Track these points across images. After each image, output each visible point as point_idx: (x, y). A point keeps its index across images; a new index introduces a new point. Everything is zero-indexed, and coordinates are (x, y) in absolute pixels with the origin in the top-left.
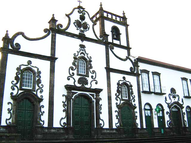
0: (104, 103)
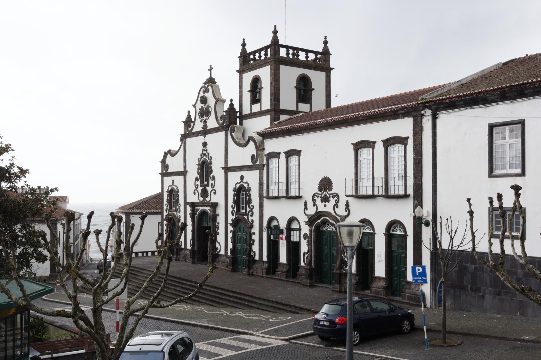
0: (221, 220)
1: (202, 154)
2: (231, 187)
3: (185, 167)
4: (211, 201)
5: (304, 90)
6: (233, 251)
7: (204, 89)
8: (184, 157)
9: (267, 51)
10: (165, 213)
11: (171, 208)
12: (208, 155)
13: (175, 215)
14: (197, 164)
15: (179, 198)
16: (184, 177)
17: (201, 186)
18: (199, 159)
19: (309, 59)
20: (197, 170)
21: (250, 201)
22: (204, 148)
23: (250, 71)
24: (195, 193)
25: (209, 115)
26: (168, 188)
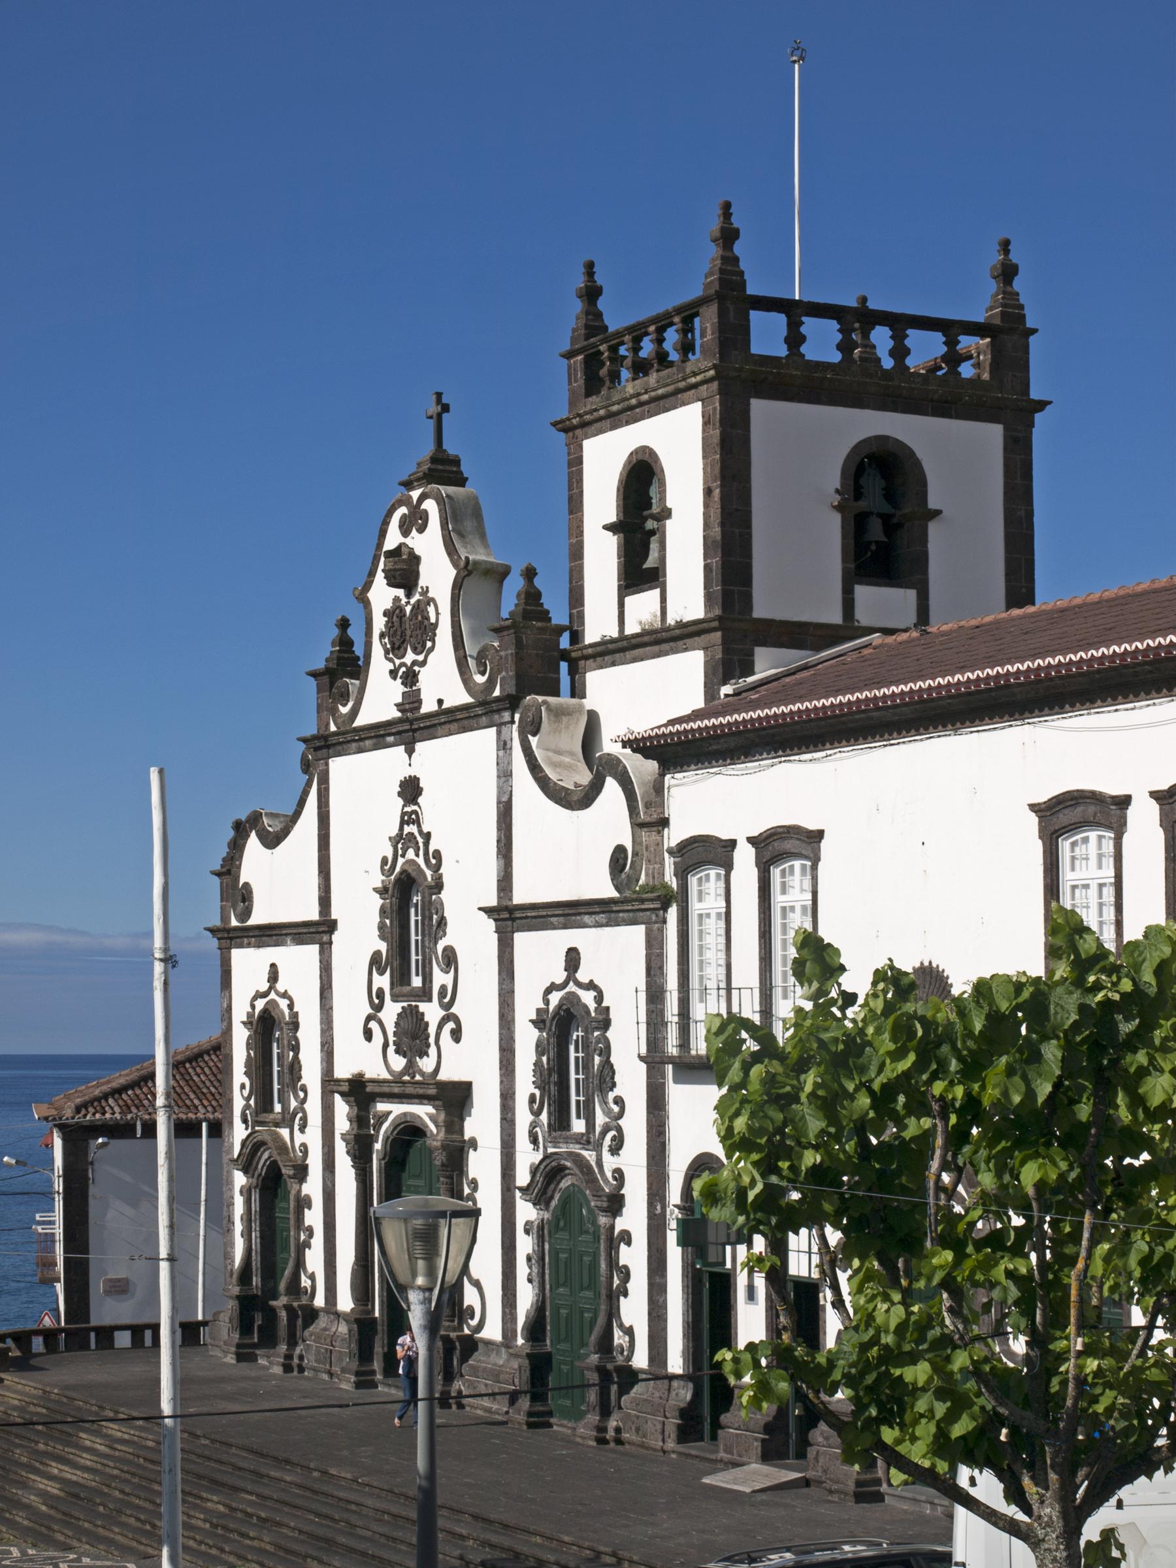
1: (400, 835)
2: (527, 1005)
3: (325, 901)
4: (443, 1076)
5: (886, 518)
6: (535, 1328)
7: (403, 510)
8: (320, 850)
9: (692, 330)
10: (239, 1133)
11: (560, 1122)
12: (427, 844)
13: (285, 1144)
14: (375, 890)
15: (301, 1056)
16: (321, 952)
17: (395, 998)
18: (384, 861)
19: (911, 362)
20: (377, 919)
21: (606, 1078)
22: (408, 809)
23: (614, 427)
24: (368, 1035)
25: (429, 644)
26: (253, 1007)
